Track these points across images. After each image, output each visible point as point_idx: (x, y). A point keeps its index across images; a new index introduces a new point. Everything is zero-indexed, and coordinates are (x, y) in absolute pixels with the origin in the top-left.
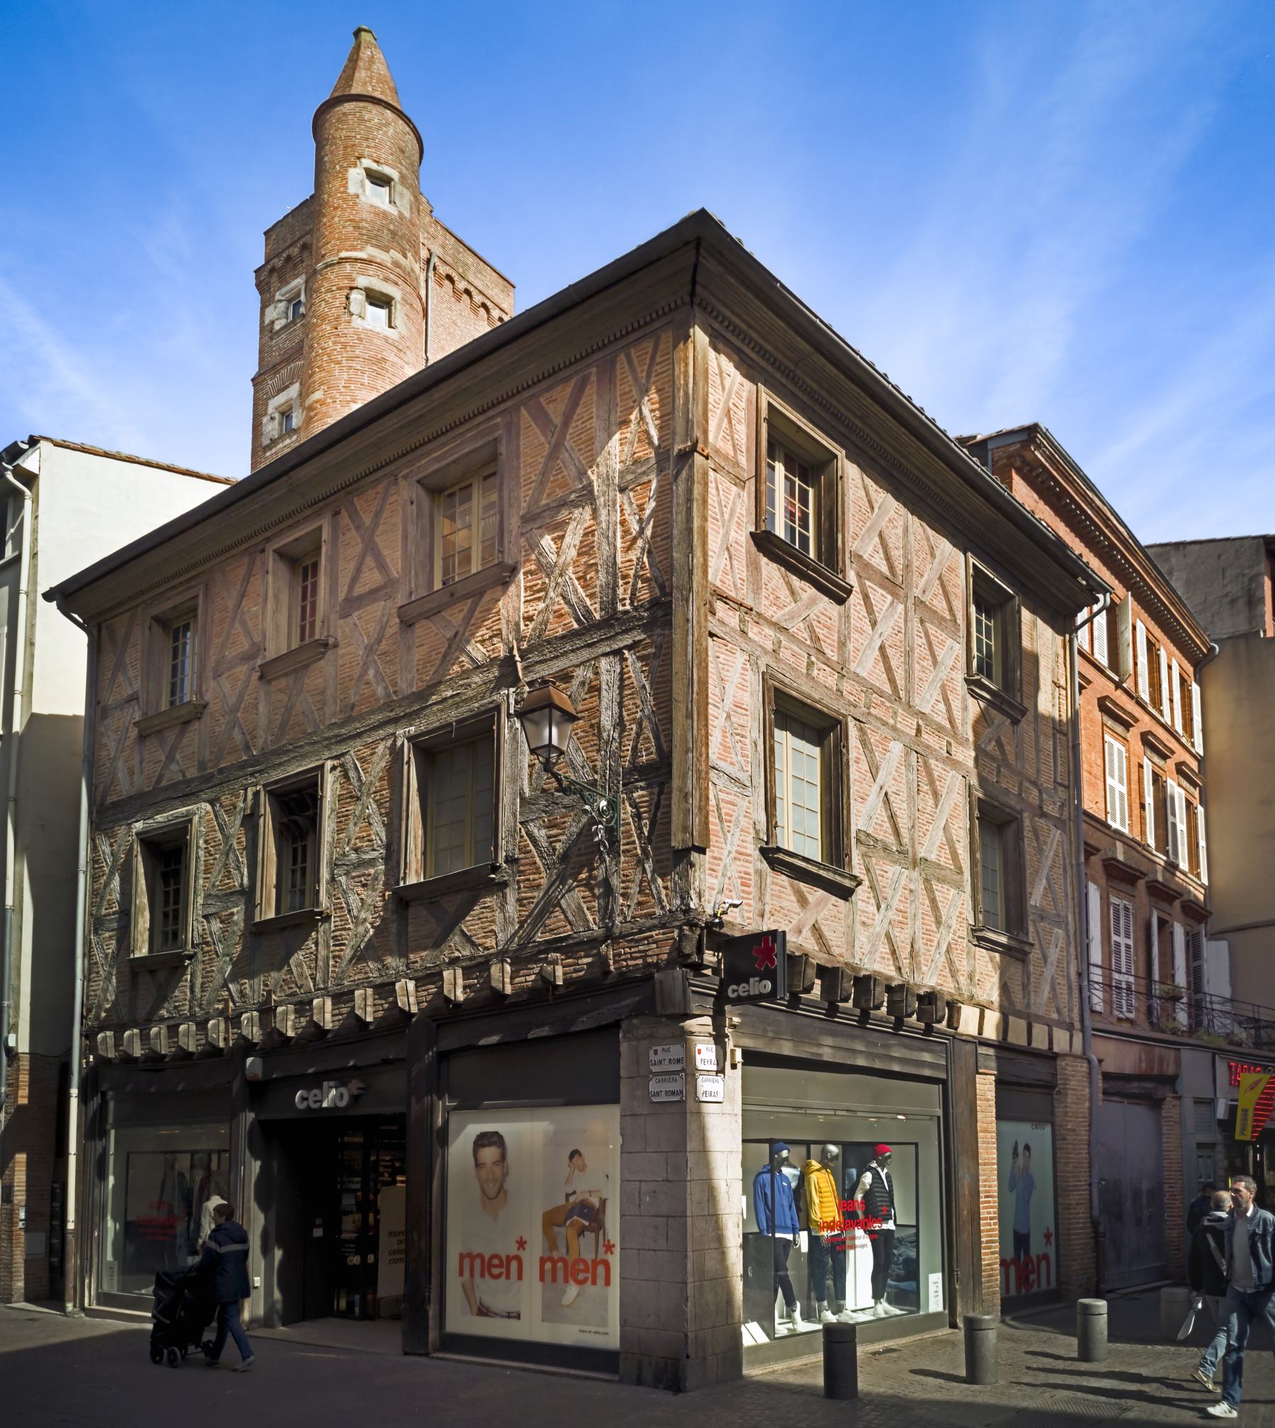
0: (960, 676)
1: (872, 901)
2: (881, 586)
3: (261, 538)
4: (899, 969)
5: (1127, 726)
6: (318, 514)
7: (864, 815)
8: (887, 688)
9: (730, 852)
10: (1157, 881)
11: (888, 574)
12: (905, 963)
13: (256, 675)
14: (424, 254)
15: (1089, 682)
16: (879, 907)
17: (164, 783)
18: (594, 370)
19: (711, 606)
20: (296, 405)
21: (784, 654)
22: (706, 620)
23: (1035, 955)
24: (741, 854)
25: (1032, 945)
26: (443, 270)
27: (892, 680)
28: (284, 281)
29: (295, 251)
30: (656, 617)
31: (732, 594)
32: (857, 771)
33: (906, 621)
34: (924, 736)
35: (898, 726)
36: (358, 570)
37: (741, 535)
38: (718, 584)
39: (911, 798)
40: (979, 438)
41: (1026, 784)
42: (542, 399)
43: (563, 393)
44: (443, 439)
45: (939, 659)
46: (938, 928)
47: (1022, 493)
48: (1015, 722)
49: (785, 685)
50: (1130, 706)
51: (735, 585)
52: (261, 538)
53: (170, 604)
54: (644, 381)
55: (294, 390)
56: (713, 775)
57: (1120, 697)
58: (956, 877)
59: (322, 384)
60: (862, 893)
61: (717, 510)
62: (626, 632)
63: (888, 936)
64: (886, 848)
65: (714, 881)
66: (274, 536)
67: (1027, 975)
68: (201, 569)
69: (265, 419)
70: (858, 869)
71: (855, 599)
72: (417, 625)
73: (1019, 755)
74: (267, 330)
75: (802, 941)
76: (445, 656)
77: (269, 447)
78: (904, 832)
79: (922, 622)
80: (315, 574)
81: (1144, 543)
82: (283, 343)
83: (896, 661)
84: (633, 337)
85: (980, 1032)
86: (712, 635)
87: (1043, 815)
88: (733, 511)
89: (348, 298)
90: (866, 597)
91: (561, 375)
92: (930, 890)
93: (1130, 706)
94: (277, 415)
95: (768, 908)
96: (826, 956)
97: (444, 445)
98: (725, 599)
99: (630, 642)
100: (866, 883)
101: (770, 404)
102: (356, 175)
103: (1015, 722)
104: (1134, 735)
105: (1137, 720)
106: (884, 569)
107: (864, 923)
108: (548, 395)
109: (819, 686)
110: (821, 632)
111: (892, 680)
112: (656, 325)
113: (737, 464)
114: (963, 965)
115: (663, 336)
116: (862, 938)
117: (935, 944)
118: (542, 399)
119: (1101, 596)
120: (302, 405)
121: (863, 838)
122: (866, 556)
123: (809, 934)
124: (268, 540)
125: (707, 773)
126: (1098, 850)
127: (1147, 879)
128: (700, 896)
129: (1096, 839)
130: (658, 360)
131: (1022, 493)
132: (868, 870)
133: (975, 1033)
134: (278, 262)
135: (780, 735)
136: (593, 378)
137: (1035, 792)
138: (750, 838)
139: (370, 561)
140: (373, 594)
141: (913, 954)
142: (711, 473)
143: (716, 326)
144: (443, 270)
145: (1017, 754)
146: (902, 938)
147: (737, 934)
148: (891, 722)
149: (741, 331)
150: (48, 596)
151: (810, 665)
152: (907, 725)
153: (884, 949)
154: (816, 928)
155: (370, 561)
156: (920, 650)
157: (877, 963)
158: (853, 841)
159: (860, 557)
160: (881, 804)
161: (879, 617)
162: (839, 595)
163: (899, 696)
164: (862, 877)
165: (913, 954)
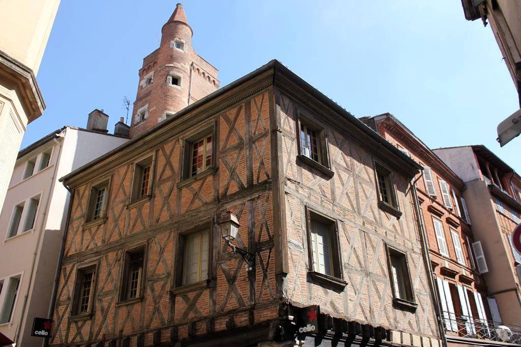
0: (375, 202)
1: (353, 291)
2: (344, 172)
3: (133, 159)
4: (366, 318)
5: (440, 216)
6: (152, 151)
7: (346, 255)
8: (350, 208)
9: (297, 274)
10: (463, 275)
11: (346, 167)
12: (368, 315)
13: (126, 207)
14: (191, 63)
15: (423, 201)
16: (356, 294)
17: (89, 248)
18: (244, 104)
19: (285, 182)
20: (147, 111)
21: (312, 198)
22: (284, 187)
23: (419, 309)
24: (301, 275)
25: (417, 305)
26: (196, 67)
27: (352, 206)
28: (147, 73)
29: (152, 64)
30: (268, 185)
31: (292, 178)
32: (343, 240)
33: (354, 183)
34: (366, 225)
35: (356, 222)
36: (164, 171)
37: (294, 158)
38: (287, 174)
39: (363, 250)
40: (371, 117)
41: (406, 241)
42: (227, 113)
43: (234, 111)
44: (195, 126)
45: (368, 196)
46: (380, 300)
47: (389, 138)
48: (398, 218)
49: (313, 209)
50: (440, 208)
51: (293, 175)
52: (133, 159)
53: (100, 182)
54: (259, 108)
55: (147, 106)
56: (289, 244)
57: (434, 204)
58: (384, 279)
59: (156, 104)
60: (348, 288)
61: (285, 149)
62: (256, 192)
63: (360, 304)
64: (356, 270)
65: (292, 286)
66: (137, 159)
67: (417, 317)
68: (111, 170)
69: (136, 116)
70: (346, 279)
71: (335, 176)
72: (183, 190)
73: (402, 230)
74: (140, 88)
75: (326, 309)
76: (192, 201)
77: (136, 125)
78: (362, 262)
79: (360, 183)
80: (149, 171)
81: (431, 149)
82: (144, 91)
83: (353, 198)
84: (256, 94)
85: (402, 343)
86: (286, 193)
87: (414, 252)
88: (291, 149)
89: (166, 78)
90: (339, 176)
91: (234, 106)
92: (375, 285)
93: (440, 208)
94: (140, 114)
95: (312, 296)
96: (337, 314)
97: (195, 128)
98: (289, 180)
99: (257, 196)
100: (350, 284)
101: (300, 113)
102: (173, 42)
103: (398, 218)
104: (443, 218)
105: (443, 214)
106: (345, 165)
107: (351, 300)
108: (229, 112)
109: (326, 210)
110: (325, 190)
111: (352, 206)
112: (263, 91)
113: (291, 133)
114: (391, 314)
115: (265, 94)
116: (351, 305)
117: (379, 307)
118: (227, 113)
119: (420, 170)
120: (148, 111)
121: (347, 265)
122: (338, 162)
123: (329, 305)
124: (134, 160)
125: (287, 244)
126: (438, 265)
127: (459, 274)
128: (286, 292)
129: (436, 260)
130: (264, 101)
131: (389, 138)
132: (350, 278)
133: (400, 343)
134: (147, 67)
135: (313, 235)
136: (244, 107)
137: (410, 244)
138: (304, 269)
139: (168, 168)
140: (168, 179)
141: (371, 311)
142: (283, 137)
143: (282, 90)
144: (196, 67)
145: (401, 230)
146: (366, 305)
147: (301, 307)
148: (353, 220)
149: (292, 96)
150: (60, 180)
151: (322, 201)
152: (359, 222)
153: (359, 310)
154: (332, 303)
155: (168, 168)
156: (361, 194)
157: (359, 318)
158: (343, 268)
159: (336, 162)
160: (352, 252)
161: (345, 182)
162: (328, 175)
163: (357, 210)
164: (347, 282)
165: (371, 311)
